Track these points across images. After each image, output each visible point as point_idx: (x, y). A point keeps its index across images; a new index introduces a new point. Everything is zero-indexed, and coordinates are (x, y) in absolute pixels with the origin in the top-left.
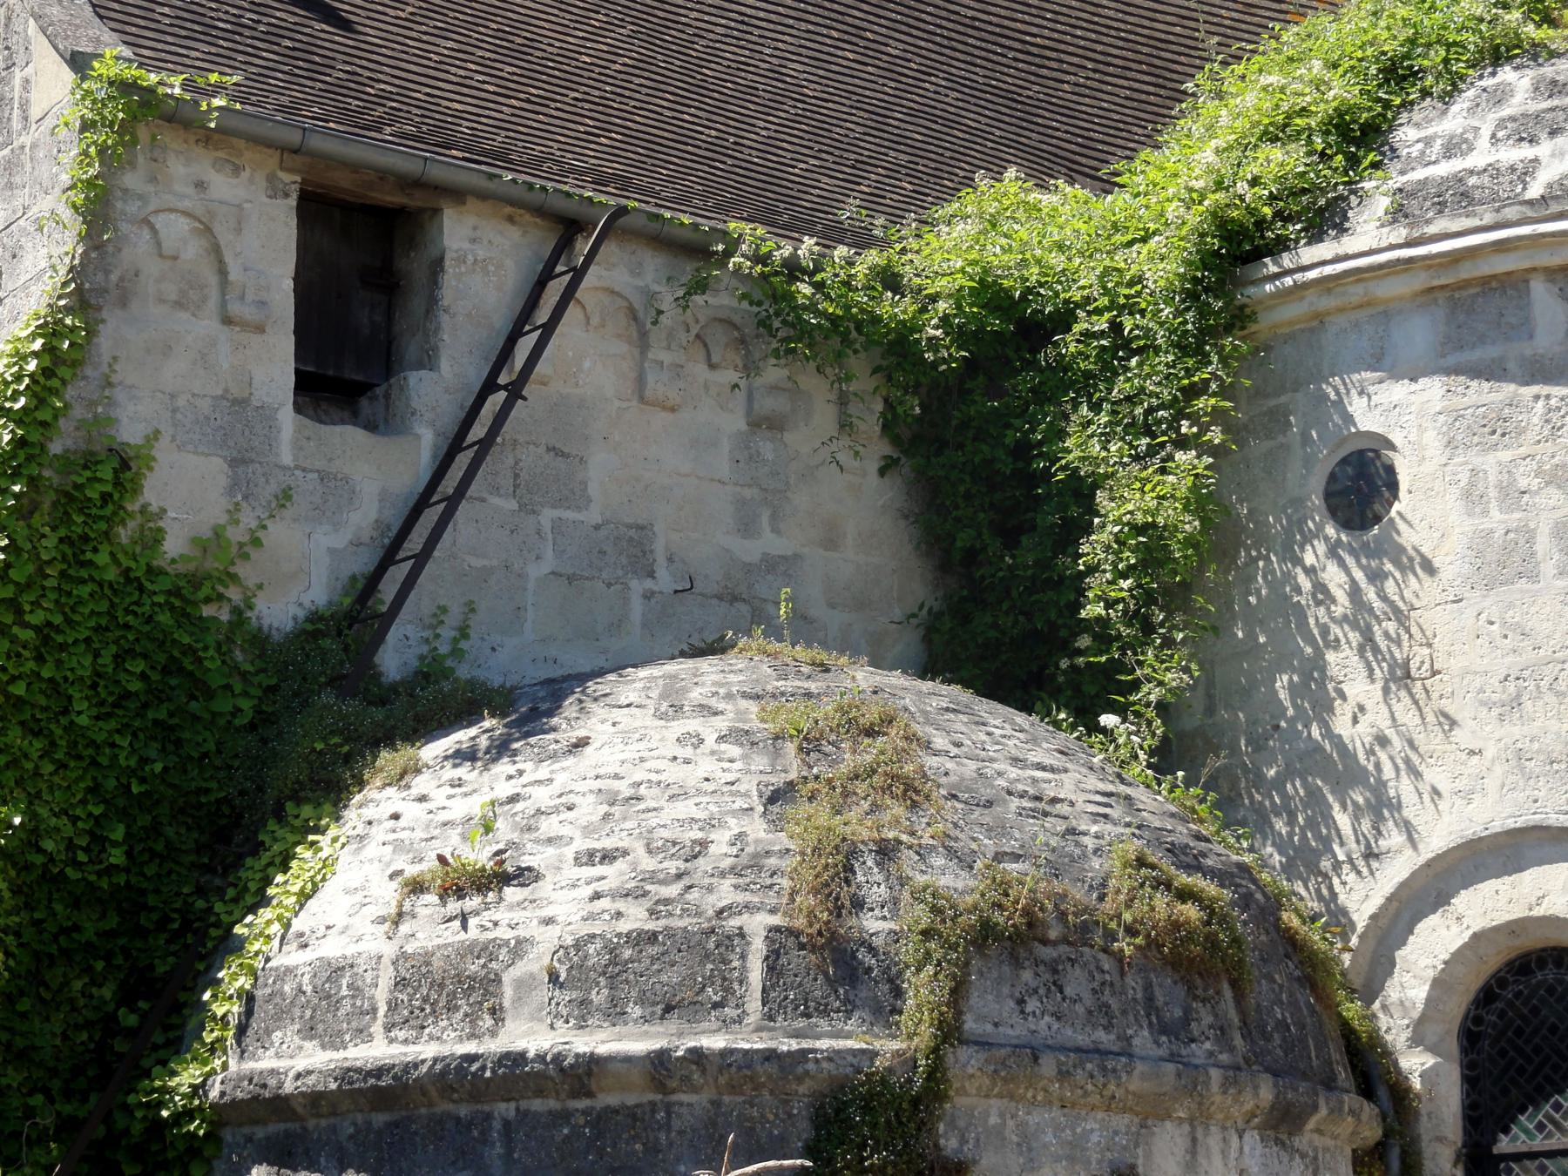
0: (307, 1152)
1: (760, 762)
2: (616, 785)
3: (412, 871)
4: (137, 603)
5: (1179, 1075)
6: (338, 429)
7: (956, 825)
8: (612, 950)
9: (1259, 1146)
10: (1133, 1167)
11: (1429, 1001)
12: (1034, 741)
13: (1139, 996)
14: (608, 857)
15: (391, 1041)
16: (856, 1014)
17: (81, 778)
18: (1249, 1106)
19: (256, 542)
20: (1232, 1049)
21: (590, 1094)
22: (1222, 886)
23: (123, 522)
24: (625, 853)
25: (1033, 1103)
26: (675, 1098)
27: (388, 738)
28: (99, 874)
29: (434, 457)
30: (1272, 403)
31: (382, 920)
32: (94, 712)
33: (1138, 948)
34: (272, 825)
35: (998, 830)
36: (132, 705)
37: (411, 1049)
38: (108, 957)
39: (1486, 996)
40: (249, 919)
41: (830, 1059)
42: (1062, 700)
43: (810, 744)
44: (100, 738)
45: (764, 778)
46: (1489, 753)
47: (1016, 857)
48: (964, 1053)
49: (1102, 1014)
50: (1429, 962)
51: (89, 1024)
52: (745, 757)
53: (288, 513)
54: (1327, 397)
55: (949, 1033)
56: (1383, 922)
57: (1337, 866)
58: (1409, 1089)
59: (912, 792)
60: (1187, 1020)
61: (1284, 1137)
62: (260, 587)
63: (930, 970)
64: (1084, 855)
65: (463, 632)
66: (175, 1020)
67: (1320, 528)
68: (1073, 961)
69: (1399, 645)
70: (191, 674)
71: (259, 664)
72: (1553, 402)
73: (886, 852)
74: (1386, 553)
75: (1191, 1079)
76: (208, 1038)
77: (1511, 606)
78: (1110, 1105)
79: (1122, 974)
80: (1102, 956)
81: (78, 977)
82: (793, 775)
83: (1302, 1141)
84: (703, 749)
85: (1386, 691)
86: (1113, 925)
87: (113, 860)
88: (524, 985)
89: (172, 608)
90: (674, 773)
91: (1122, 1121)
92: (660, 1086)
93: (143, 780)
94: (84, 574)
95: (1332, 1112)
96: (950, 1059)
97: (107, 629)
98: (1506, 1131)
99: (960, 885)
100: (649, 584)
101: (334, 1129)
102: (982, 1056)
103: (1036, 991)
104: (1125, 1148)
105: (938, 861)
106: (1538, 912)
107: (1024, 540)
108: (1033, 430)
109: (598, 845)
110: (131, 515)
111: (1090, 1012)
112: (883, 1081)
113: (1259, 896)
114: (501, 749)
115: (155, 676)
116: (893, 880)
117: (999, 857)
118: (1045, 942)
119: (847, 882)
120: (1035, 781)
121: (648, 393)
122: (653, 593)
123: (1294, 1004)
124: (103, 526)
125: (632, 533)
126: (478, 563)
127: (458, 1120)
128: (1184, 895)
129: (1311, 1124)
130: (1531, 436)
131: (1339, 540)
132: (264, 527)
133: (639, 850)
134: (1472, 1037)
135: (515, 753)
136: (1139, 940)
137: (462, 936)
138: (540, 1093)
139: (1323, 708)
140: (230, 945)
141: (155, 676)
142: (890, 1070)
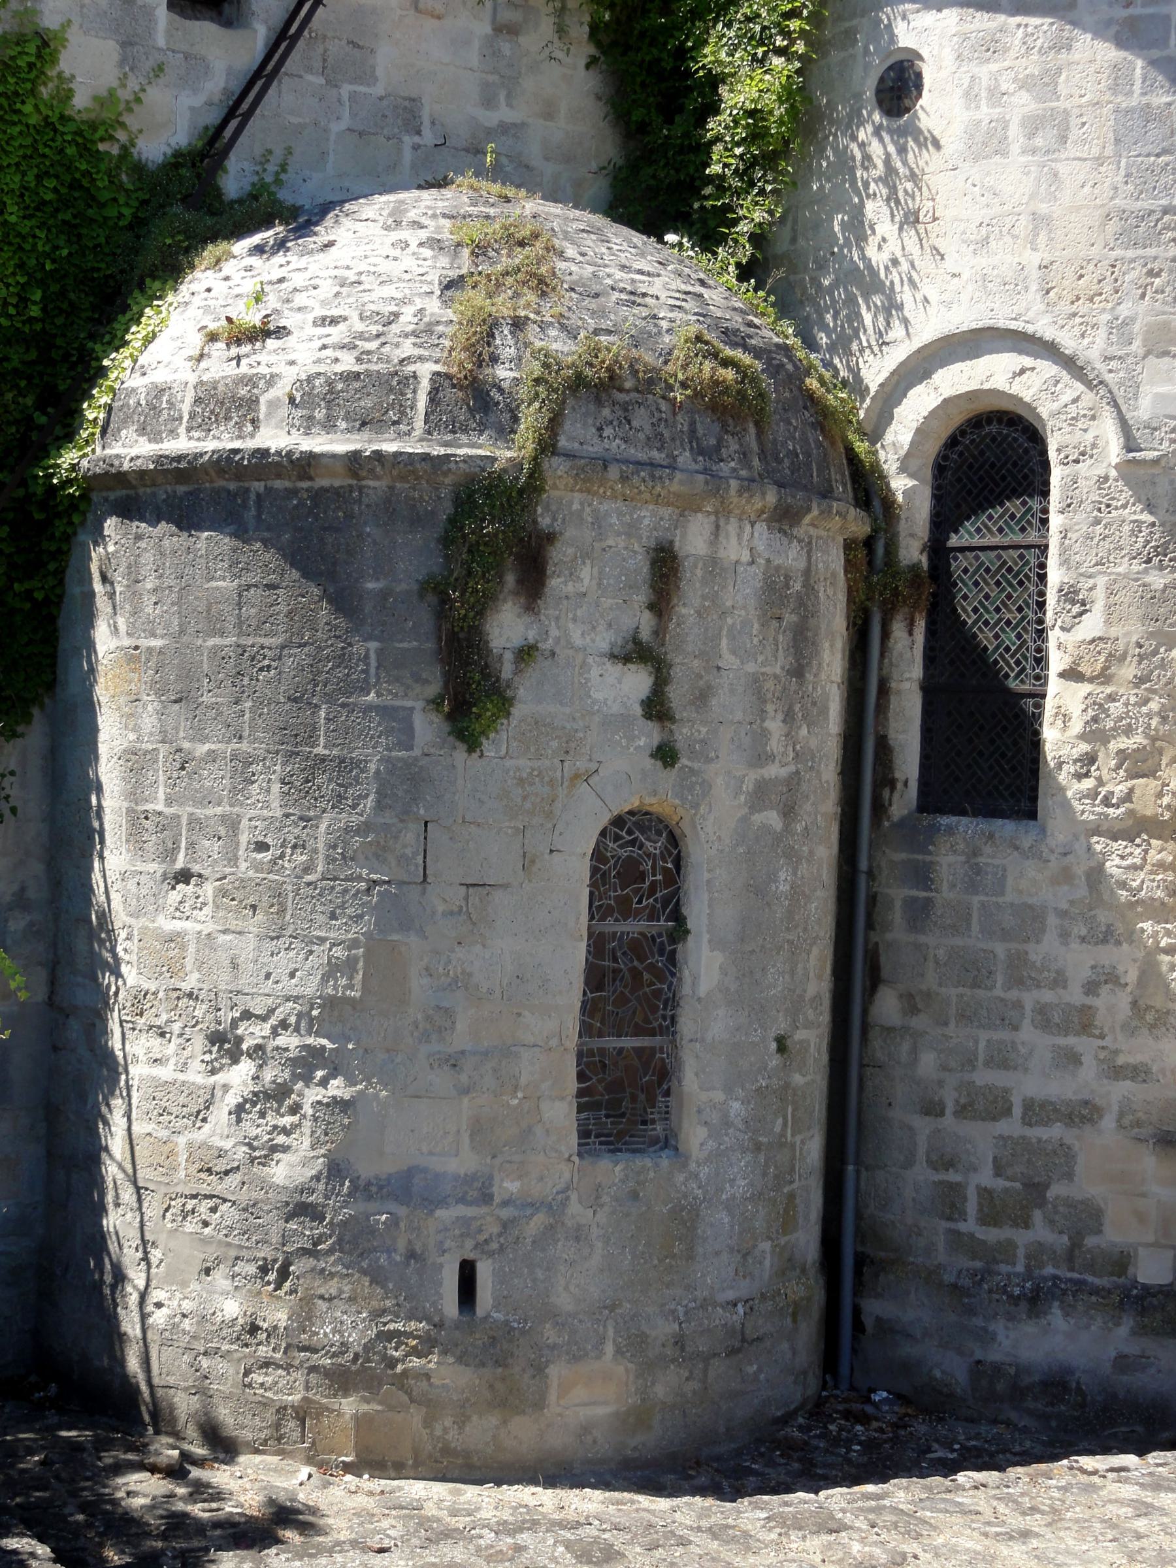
0: (139, 509)
1: (444, 261)
2: (347, 273)
3: (213, 327)
4: (53, 140)
5: (707, 483)
6: (198, 23)
7: (570, 309)
8: (330, 383)
9: (766, 533)
10: (672, 542)
11: (912, 443)
12: (642, 255)
13: (686, 429)
14: (334, 321)
15: (190, 438)
16: (487, 433)
17: (9, 259)
18: (759, 505)
19: (138, 100)
20: (750, 468)
21: (311, 479)
22: (755, 357)
23: (45, 84)
24: (345, 319)
25: (604, 496)
26: (364, 483)
27: (214, 236)
28: (24, 323)
29: (266, 45)
30: (847, 24)
31: (190, 358)
32: (21, 213)
33: (688, 397)
34: (136, 293)
35: (600, 313)
36: (48, 209)
37: (202, 444)
38: (29, 378)
39: (952, 442)
40: (113, 355)
41: (465, 461)
42: (694, 229)
43: (480, 250)
44: (24, 231)
45: (445, 272)
46: (964, 277)
47: (609, 332)
48: (556, 461)
49: (657, 440)
50: (915, 417)
51: (17, 422)
52: (434, 257)
53: (161, 81)
54: (882, 21)
55: (547, 446)
56: (886, 389)
57: (862, 350)
58: (894, 501)
59: (543, 286)
60: (718, 447)
61: (786, 528)
62: (141, 131)
63: (537, 405)
64: (660, 333)
65: (283, 168)
66: (69, 420)
67: (870, 114)
68: (640, 404)
69: (913, 199)
70: (88, 189)
71: (138, 184)
72: (1030, 30)
73: (518, 324)
74: (911, 134)
75: (716, 485)
76: (85, 435)
77: (989, 173)
78: (657, 499)
79: (674, 414)
80: (661, 401)
81: (10, 390)
82: (464, 271)
83: (800, 531)
84: (409, 251)
85: (901, 229)
86: (671, 381)
87: (32, 314)
88: (273, 405)
89: (77, 144)
90: (385, 267)
91: (665, 512)
92: (355, 474)
93: (54, 261)
94: (15, 118)
95: (822, 513)
96: (545, 465)
97: (31, 157)
98: (956, 532)
99: (566, 349)
100: (416, 139)
101: (154, 494)
102: (569, 464)
103: (611, 422)
104: (668, 529)
105: (553, 332)
106: (986, 386)
107: (677, 118)
108: (687, 39)
109: (329, 313)
110: (50, 79)
111: (649, 439)
112: (499, 476)
113: (790, 367)
114: (281, 245)
115: (64, 191)
116: (520, 344)
117: (597, 332)
118: (621, 390)
119: (489, 344)
120: (633, 281)
121: (421, 6)
122: (419, 146)
123: (805, 440)
124: (29, 86)
125: (407, 103)
126: (295, 120)
127: (229, 492)
128: (726, 363)
129: (807, 519)
130: (1012, 54)
131: (881, 125)
132: (144, 90)
133: (354, 316)
134: (940, 468)
135: (288, 249)
136: (689, 392)
137: (237, 371)
138: (279, 476)
139: (862, 238)
140: (102, 372)
141: (64, 191)
142: (505, 470)
